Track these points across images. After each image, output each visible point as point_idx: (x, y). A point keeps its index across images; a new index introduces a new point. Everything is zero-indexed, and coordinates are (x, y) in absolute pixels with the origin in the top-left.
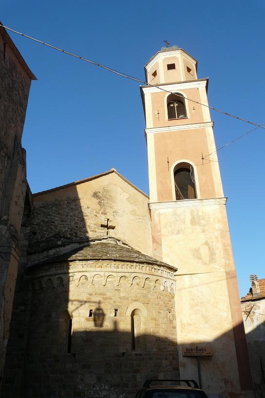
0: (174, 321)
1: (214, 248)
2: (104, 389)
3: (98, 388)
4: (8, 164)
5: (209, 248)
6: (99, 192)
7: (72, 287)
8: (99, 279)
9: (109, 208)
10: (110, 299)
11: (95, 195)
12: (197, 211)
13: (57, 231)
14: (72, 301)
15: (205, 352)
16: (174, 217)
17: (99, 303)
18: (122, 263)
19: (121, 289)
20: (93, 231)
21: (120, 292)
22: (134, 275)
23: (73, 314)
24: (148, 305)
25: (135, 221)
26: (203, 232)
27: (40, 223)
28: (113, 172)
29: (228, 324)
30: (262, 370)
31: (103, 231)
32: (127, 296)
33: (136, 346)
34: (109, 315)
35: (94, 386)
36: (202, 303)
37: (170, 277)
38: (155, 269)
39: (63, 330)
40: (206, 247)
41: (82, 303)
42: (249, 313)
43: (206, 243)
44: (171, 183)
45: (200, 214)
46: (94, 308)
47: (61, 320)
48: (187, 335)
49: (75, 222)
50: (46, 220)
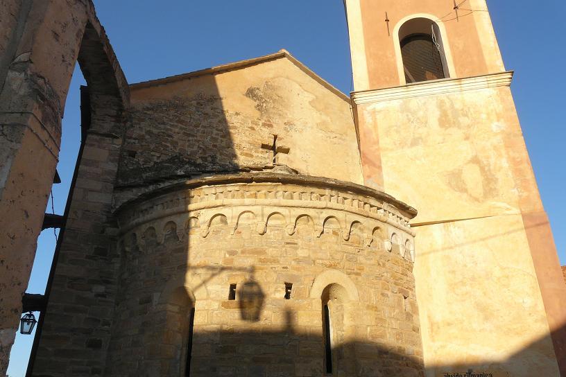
0: (415, 316)
1: (492, 167)
5: (482, 169)
6: (258, 89)
7: (195, 239)
8: (250, 222)
10: (275, 261)
11: (251, 93)
14: (195, 268)
17: (252, 270)
18: (300, 189)
19: (300, 242)
20: (246, 155)
21: (297, 249)
22: (326, 214)
23: (196, 294)
24: (360, 278)
25: (326, 141)
26: (467, 138)
27: (143, 136)
28: (283, 56)
31: (266, 155)
32: (313, 256)
33: (334, 364)
34: (272, 296)
36: (473, 279)
37: (403, 227)
38: (371, 206)
39: (176, 329)
41: (214, 272)
43: (475, 160)
44: (394, 55)
45: (458, 106)
46: (239, 281)
47: (170, 307)
49: (212, 138)
50: (155, 131)
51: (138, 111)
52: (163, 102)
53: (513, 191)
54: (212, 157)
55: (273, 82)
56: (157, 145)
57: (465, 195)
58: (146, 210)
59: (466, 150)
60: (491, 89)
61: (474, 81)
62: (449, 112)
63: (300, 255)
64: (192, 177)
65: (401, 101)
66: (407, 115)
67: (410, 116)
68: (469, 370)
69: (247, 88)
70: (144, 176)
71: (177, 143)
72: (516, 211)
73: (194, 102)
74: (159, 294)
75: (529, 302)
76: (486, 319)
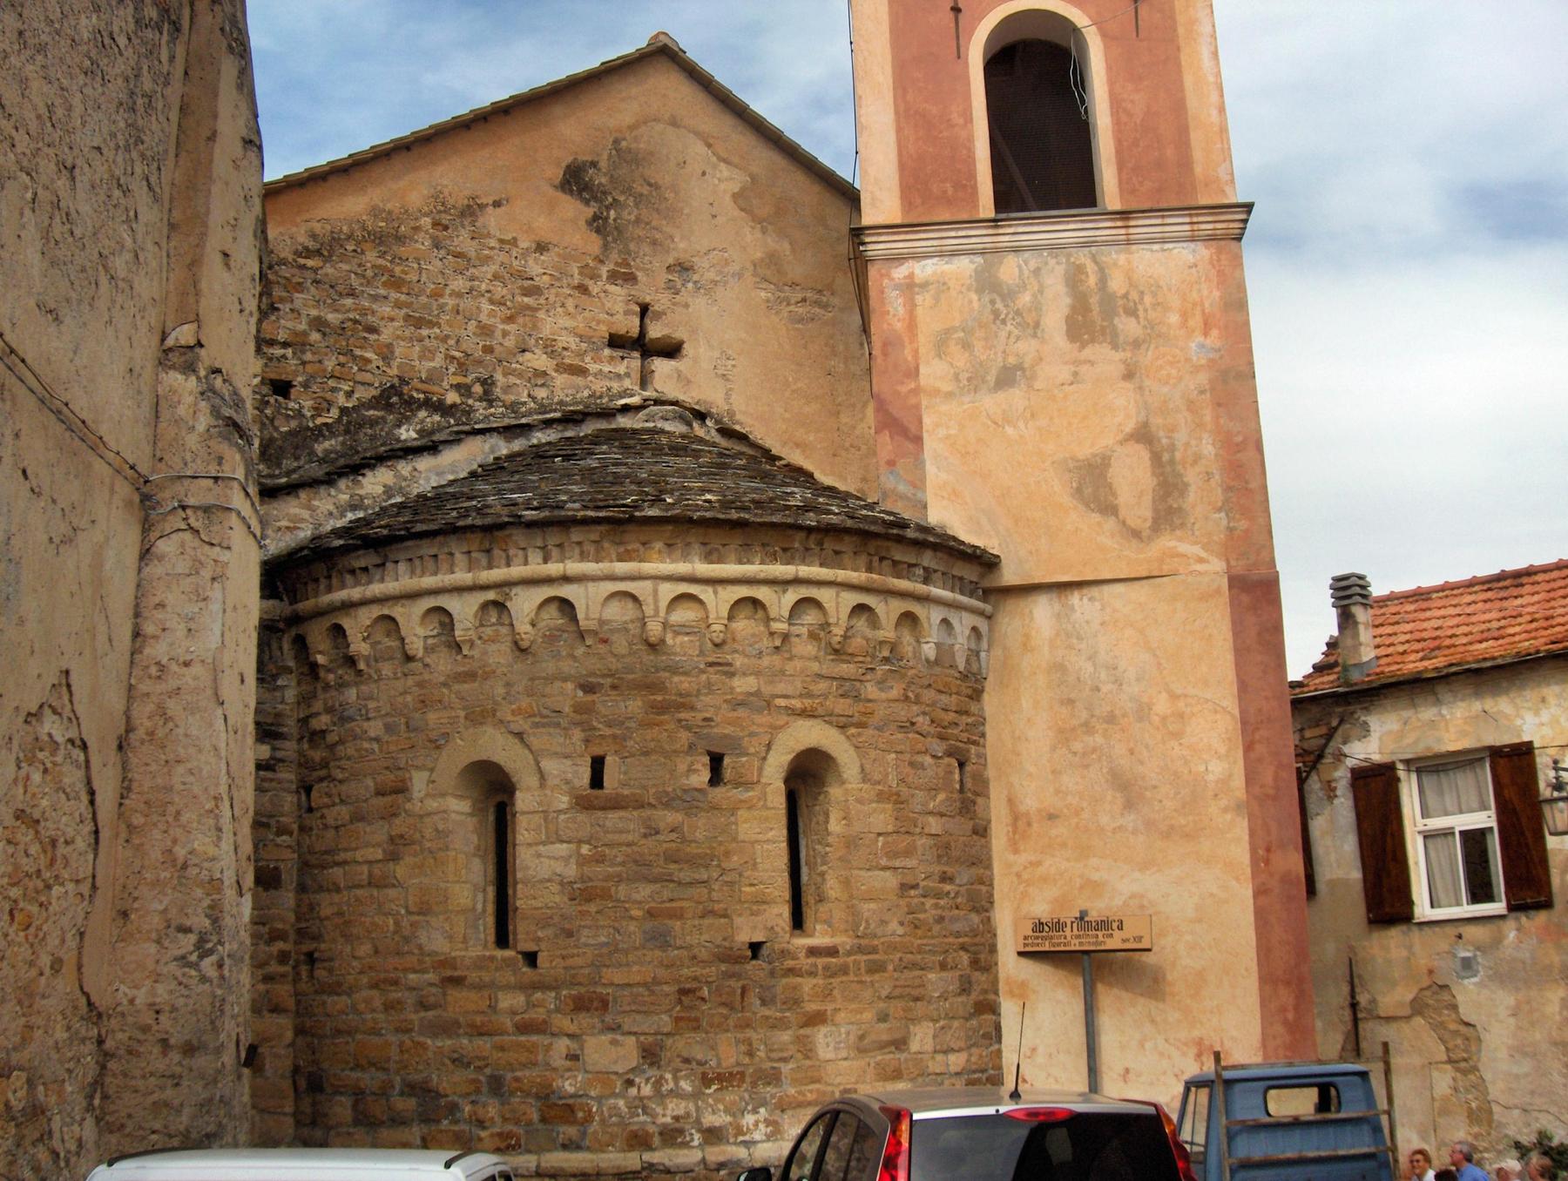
0: (980, 800)
1: (1178, 455)
2: (676, 1093)
3: (647, 1090)
4: (172, 58)
5: (1156, 458)
6: (594, 164)
9: (646, 248)
12: (1101, 269)
13: (394, 371)
15: (1116, 933)
16: (986, 299)
26: (1129, 375)
27: (305, 334)
29: (1225, 810)
30: (1354, 1006)
31: (621, 368)
33: (809, 914)
35: (630, 1083)
36: (1111, 719)
40: (1141, 454)
42: (1320, 756)
43: (1143, 435)
44: (969, 120)
45: (1117, 284)
48: (1039, 863)
50: (332, 318)
51: (283, 262)
52: (345, 229)
53: (1217, 515)
54: (484, 382)
55: (636, 139)
56: (342, 359)
57: (1110, 523)
58: (365, 569)
59: (1123, 409)
60: (1200, 246)
61: (1159, 221)
62: (1094, 301)
63: (738, 690)
64: (441, 448)
65: (979, 259)
66: (993, 302)
67: (999, 305)
68: (1081, 912)
69: (564, 165)
70: (321, 448)
71: (390, 346)
72: (1217, 565)
73: (426, 222)
74: (426, 774)
75: (1217, 769)
76: (1129, 805)
